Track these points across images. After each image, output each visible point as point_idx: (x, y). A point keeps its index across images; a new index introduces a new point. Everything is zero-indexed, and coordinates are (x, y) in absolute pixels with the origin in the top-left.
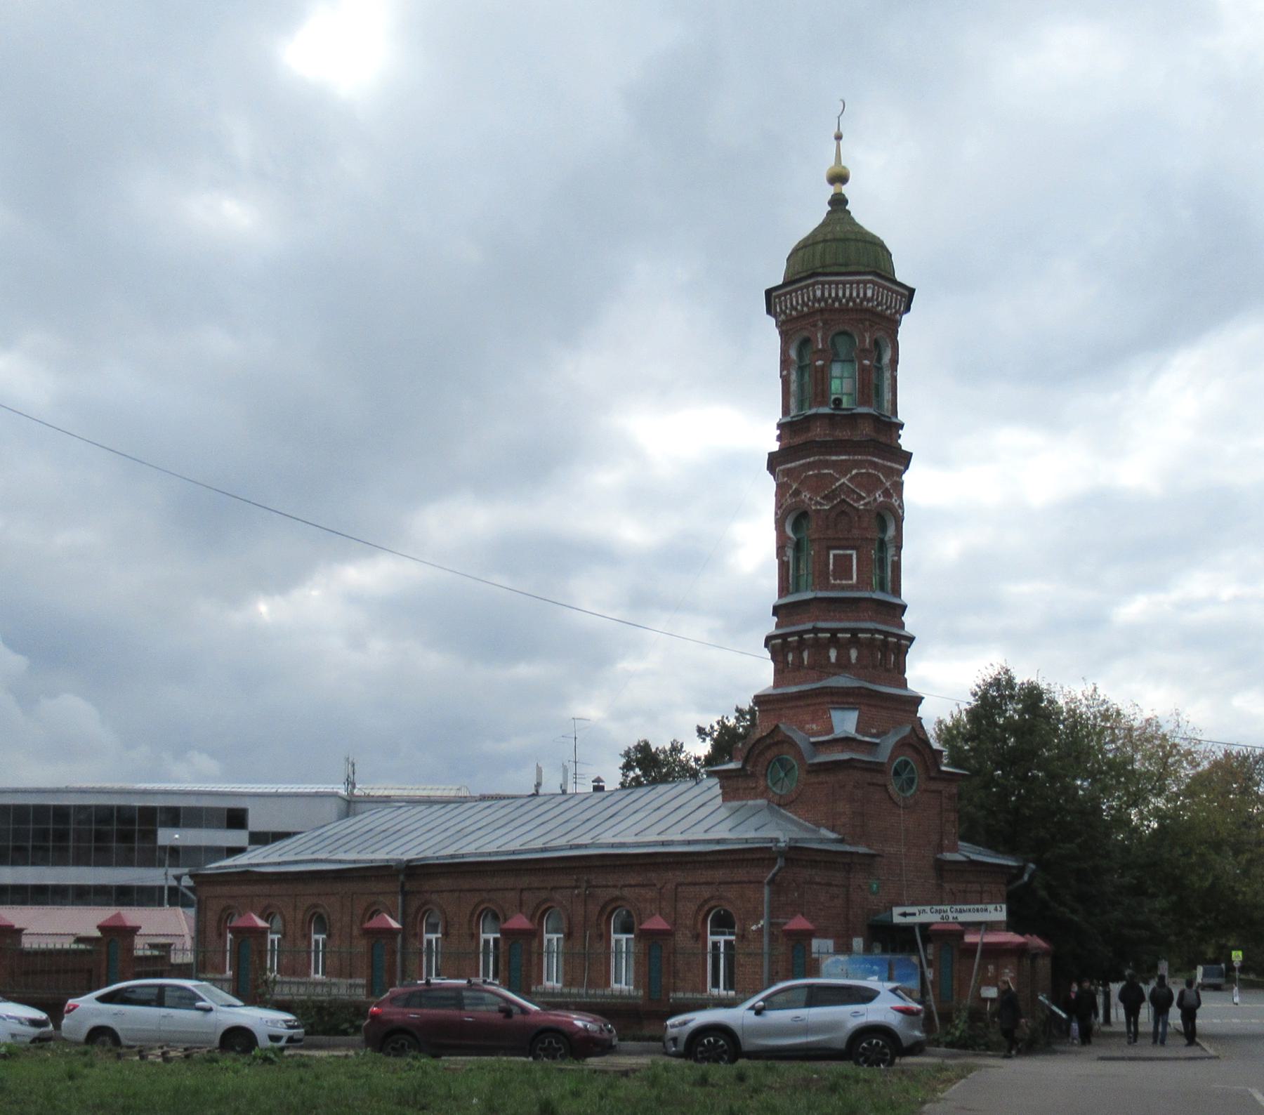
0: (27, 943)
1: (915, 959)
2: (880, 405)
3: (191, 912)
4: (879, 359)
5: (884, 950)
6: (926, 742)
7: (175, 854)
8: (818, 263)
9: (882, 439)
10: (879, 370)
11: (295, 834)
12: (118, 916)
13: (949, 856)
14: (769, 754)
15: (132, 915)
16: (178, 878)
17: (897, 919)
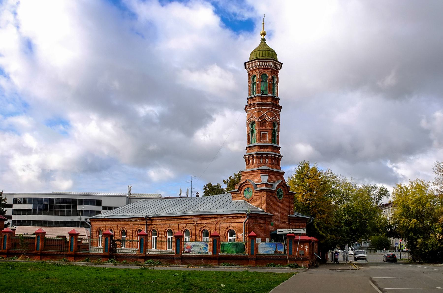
0: (47, 237)
1: (282, 243)
2: (274, 94)
3: (89, 229)
4: (274, 81)
5: (275, 241)
6: (286, 185)
7: (83, 213)
8: (258, 56)
9: (274, 103)
10: (274, 84)
11: (115, 208)
12: (74, 230)
13: (291, 215)
14: (245, 188)
15: (44, 229)
16: (86, 220)
17: (278, 233)
